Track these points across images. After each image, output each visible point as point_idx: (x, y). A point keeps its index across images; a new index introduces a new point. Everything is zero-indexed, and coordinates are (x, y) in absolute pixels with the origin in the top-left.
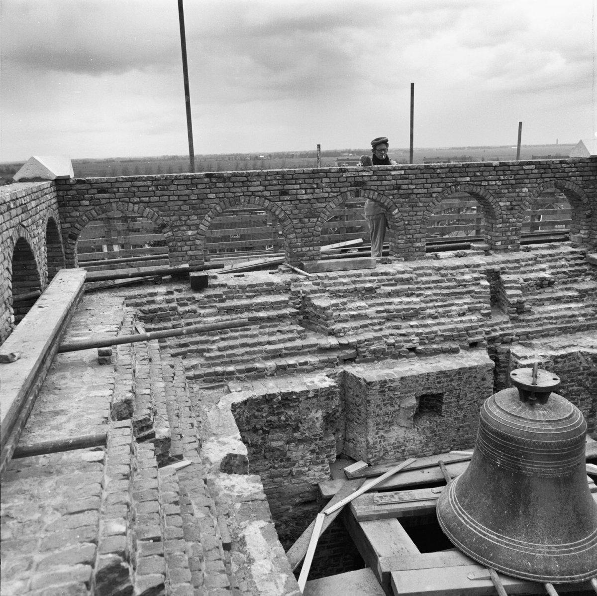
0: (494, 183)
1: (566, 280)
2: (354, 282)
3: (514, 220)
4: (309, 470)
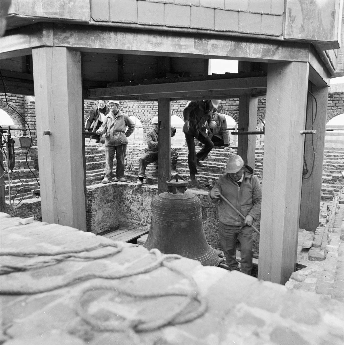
1: (333, 171)
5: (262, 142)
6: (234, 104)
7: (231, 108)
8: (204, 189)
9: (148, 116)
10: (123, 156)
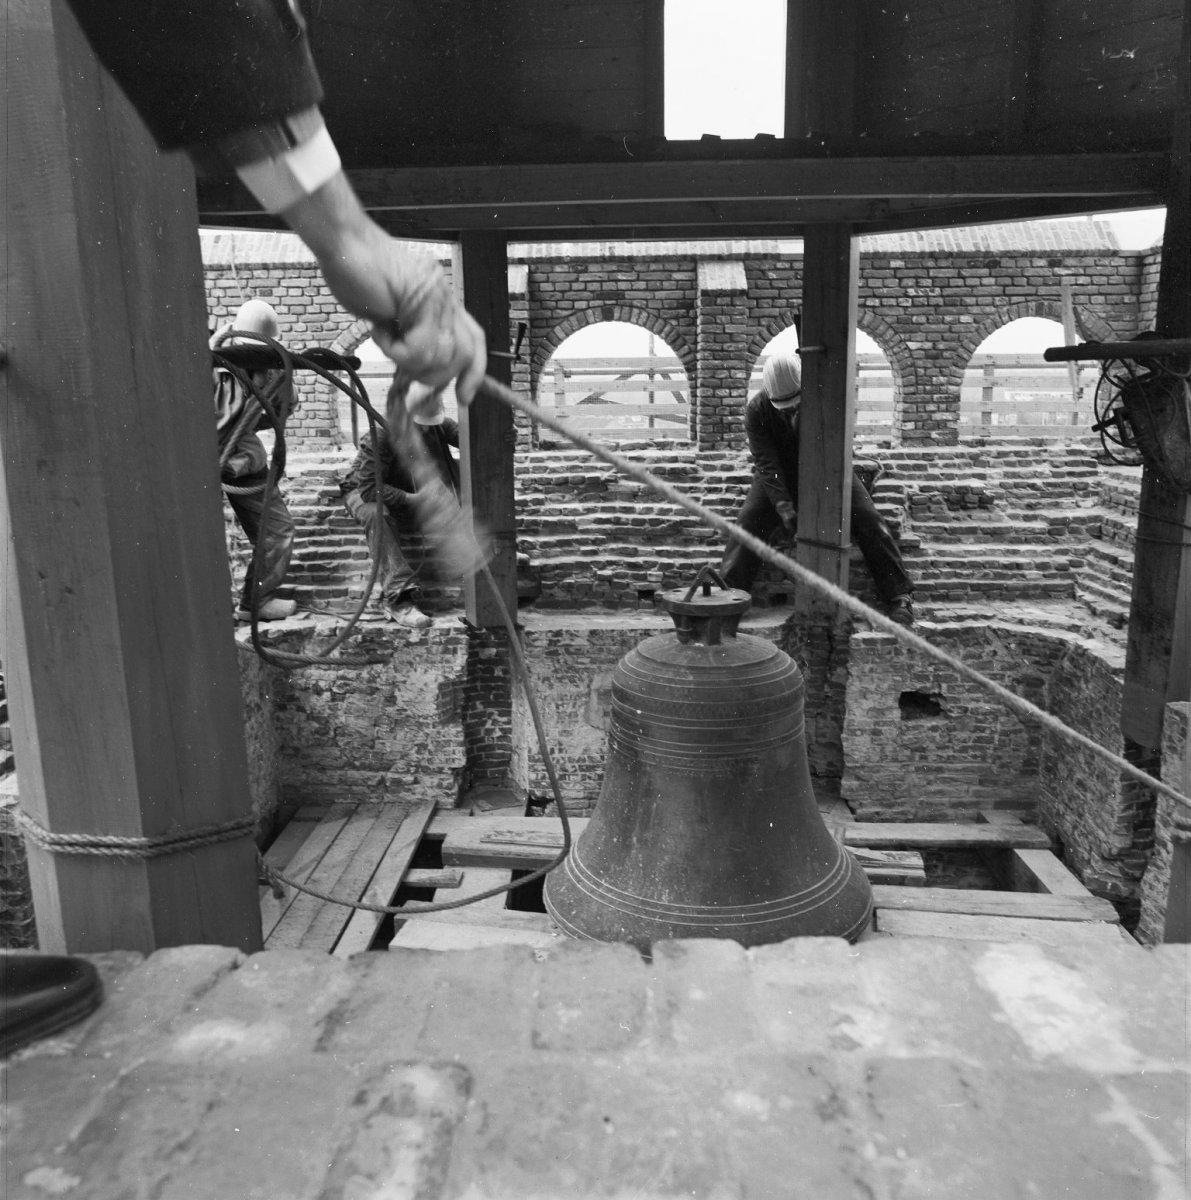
0: (893, 301)
1: (1033, 501)
2: (572, 469)
3: (942, 379)
4: (416, 782)
5: (657, 416)
6: (666, 284)
7: (654, 298)
8: (635, 607)
9: (291, 330)
10: (694, 524)
